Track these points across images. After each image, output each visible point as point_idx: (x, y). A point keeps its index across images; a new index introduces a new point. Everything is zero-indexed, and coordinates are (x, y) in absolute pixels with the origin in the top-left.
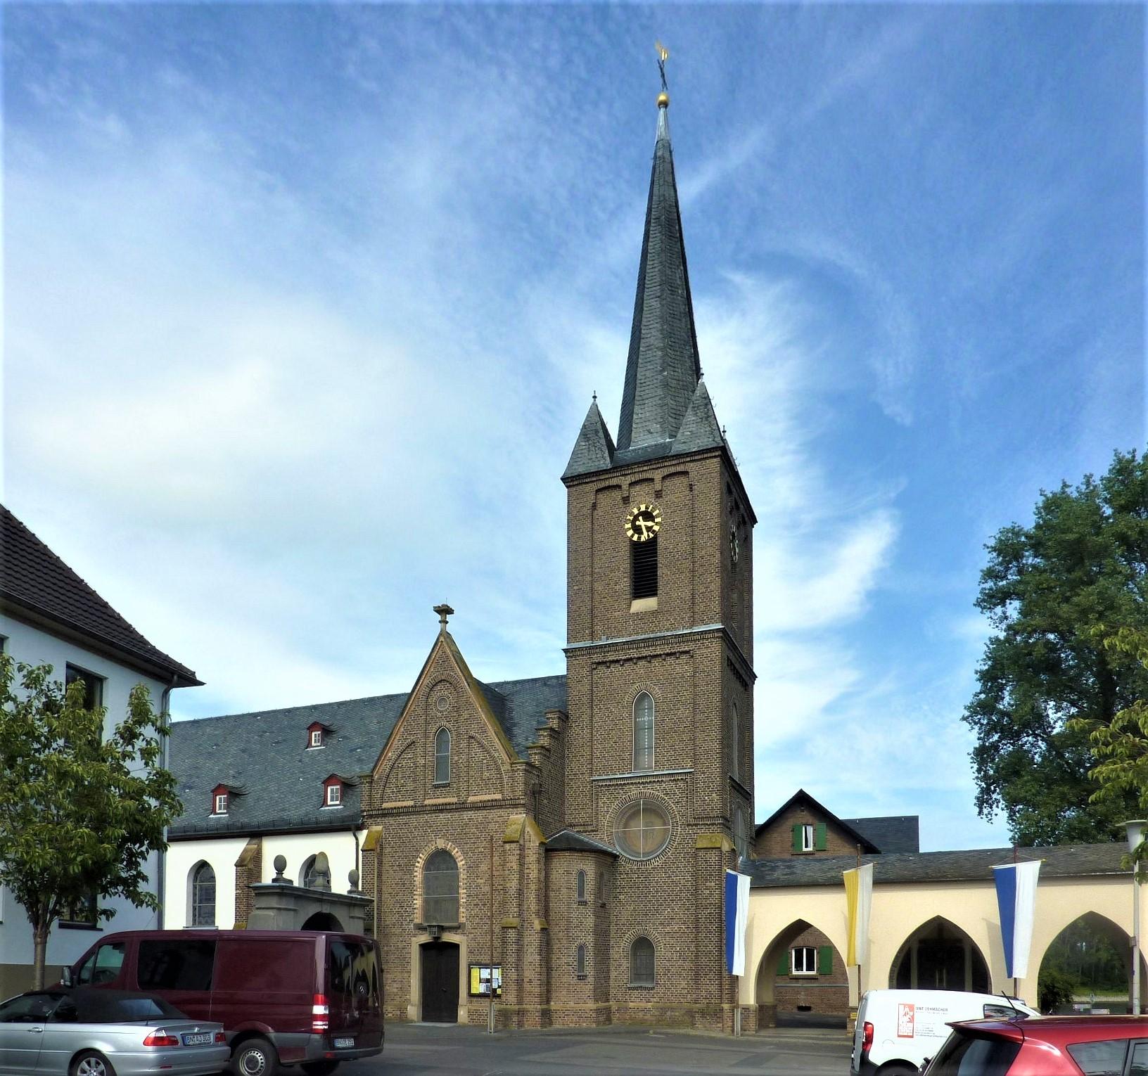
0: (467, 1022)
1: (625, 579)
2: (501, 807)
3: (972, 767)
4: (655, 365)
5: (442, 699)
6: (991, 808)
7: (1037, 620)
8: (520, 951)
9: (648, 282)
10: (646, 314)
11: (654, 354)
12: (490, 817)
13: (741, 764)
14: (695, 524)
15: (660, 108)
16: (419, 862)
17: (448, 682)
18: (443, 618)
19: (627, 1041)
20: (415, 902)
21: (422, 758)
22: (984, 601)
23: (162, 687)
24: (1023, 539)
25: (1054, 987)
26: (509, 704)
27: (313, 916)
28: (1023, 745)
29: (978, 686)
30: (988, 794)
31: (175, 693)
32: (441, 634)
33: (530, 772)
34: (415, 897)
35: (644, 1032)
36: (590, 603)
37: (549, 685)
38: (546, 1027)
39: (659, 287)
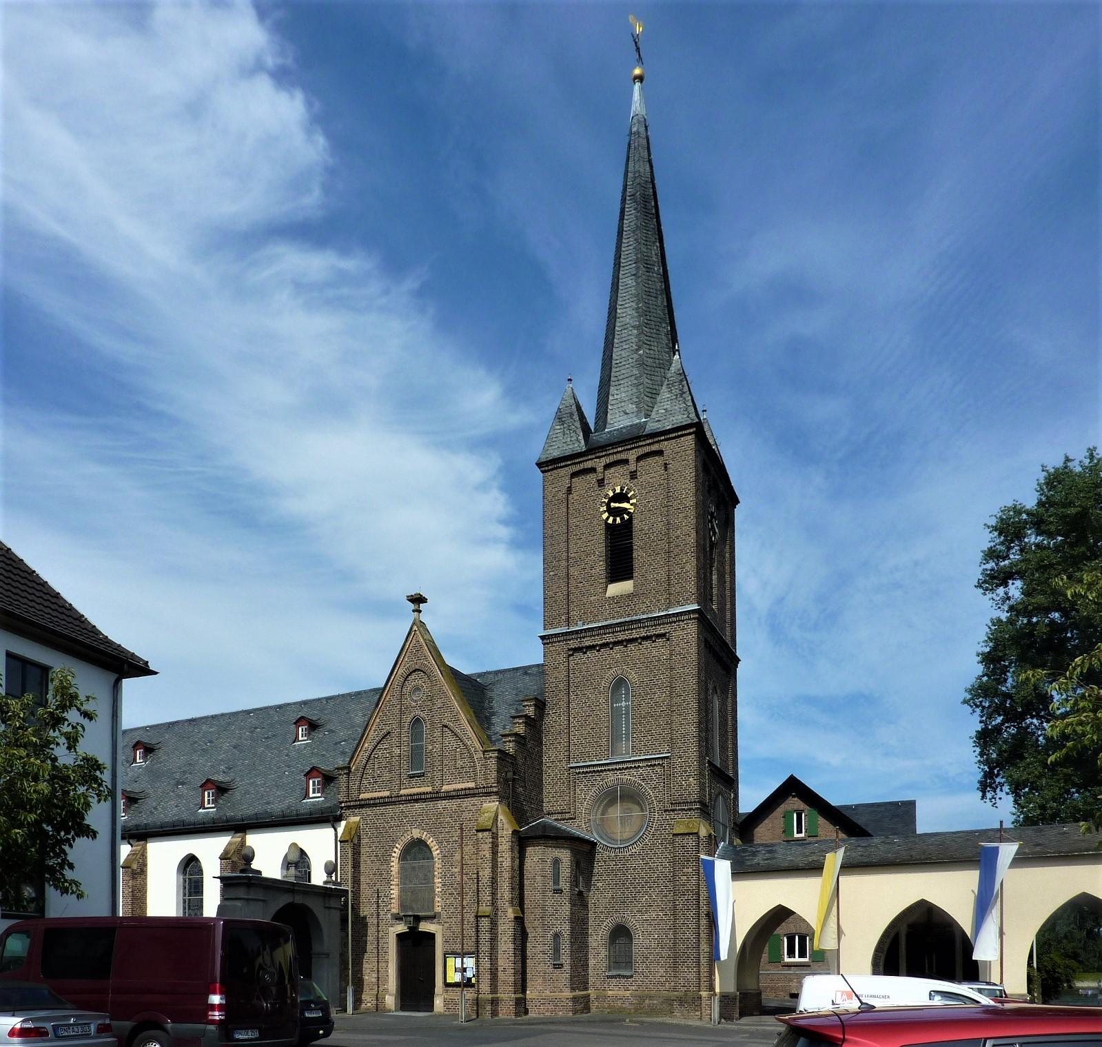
0: (442, 1011)
1: (601, 563)
2: (474, 795)
3: (974, 751)
4: (631, 344)
5: (417, 689)
6: (995, 792)
7: (1040, 599)
8: (494, 940)
9: (624, 261)
10: (621, 293)
11: (630, 333)
12: (463, 805)
13: (724, 748)
14: (670, 504)
15: (635, 83)
16: (395, 852)
17: (422, 671)
18: (417, 607)
19: (600, 1030)
20: (392, 892)
21: (399, 748)
22: (985, 582)
23: (114, 676)
24: (1024, 516)
25: (1055, 972)
26: (489, 694)
27: (284, 906)
28: (1028, 727)
29: (980, 669)
30: (991, 778)
31: (127, 683)
32: (414, 624)
33: (503, 760)
34: (392, 887)
35: (619, 1020)
36: (565, 588)
37: (530, 674)
38: (520, 1016)
39: (634, 265)
